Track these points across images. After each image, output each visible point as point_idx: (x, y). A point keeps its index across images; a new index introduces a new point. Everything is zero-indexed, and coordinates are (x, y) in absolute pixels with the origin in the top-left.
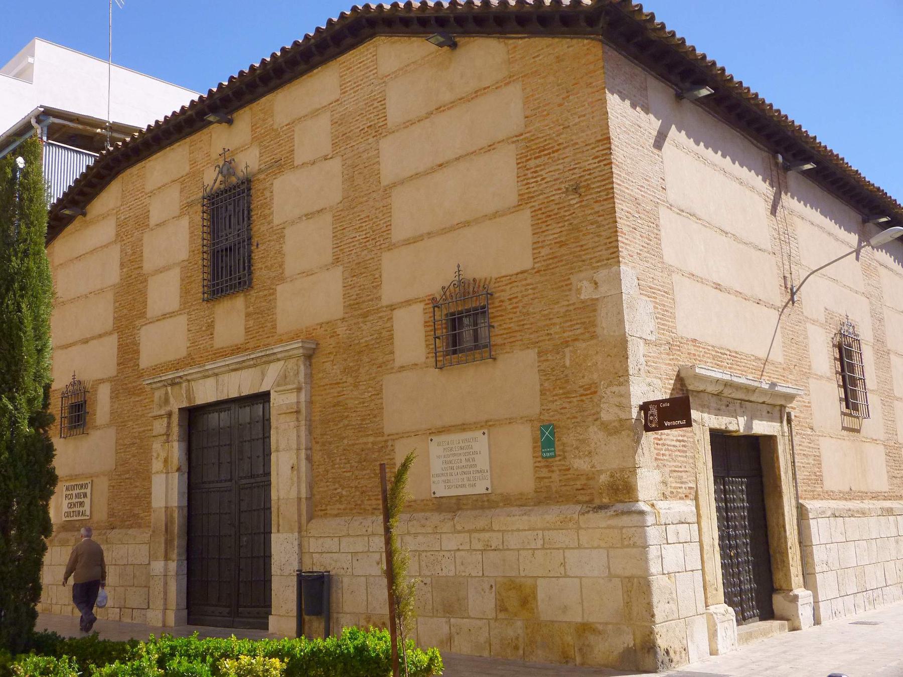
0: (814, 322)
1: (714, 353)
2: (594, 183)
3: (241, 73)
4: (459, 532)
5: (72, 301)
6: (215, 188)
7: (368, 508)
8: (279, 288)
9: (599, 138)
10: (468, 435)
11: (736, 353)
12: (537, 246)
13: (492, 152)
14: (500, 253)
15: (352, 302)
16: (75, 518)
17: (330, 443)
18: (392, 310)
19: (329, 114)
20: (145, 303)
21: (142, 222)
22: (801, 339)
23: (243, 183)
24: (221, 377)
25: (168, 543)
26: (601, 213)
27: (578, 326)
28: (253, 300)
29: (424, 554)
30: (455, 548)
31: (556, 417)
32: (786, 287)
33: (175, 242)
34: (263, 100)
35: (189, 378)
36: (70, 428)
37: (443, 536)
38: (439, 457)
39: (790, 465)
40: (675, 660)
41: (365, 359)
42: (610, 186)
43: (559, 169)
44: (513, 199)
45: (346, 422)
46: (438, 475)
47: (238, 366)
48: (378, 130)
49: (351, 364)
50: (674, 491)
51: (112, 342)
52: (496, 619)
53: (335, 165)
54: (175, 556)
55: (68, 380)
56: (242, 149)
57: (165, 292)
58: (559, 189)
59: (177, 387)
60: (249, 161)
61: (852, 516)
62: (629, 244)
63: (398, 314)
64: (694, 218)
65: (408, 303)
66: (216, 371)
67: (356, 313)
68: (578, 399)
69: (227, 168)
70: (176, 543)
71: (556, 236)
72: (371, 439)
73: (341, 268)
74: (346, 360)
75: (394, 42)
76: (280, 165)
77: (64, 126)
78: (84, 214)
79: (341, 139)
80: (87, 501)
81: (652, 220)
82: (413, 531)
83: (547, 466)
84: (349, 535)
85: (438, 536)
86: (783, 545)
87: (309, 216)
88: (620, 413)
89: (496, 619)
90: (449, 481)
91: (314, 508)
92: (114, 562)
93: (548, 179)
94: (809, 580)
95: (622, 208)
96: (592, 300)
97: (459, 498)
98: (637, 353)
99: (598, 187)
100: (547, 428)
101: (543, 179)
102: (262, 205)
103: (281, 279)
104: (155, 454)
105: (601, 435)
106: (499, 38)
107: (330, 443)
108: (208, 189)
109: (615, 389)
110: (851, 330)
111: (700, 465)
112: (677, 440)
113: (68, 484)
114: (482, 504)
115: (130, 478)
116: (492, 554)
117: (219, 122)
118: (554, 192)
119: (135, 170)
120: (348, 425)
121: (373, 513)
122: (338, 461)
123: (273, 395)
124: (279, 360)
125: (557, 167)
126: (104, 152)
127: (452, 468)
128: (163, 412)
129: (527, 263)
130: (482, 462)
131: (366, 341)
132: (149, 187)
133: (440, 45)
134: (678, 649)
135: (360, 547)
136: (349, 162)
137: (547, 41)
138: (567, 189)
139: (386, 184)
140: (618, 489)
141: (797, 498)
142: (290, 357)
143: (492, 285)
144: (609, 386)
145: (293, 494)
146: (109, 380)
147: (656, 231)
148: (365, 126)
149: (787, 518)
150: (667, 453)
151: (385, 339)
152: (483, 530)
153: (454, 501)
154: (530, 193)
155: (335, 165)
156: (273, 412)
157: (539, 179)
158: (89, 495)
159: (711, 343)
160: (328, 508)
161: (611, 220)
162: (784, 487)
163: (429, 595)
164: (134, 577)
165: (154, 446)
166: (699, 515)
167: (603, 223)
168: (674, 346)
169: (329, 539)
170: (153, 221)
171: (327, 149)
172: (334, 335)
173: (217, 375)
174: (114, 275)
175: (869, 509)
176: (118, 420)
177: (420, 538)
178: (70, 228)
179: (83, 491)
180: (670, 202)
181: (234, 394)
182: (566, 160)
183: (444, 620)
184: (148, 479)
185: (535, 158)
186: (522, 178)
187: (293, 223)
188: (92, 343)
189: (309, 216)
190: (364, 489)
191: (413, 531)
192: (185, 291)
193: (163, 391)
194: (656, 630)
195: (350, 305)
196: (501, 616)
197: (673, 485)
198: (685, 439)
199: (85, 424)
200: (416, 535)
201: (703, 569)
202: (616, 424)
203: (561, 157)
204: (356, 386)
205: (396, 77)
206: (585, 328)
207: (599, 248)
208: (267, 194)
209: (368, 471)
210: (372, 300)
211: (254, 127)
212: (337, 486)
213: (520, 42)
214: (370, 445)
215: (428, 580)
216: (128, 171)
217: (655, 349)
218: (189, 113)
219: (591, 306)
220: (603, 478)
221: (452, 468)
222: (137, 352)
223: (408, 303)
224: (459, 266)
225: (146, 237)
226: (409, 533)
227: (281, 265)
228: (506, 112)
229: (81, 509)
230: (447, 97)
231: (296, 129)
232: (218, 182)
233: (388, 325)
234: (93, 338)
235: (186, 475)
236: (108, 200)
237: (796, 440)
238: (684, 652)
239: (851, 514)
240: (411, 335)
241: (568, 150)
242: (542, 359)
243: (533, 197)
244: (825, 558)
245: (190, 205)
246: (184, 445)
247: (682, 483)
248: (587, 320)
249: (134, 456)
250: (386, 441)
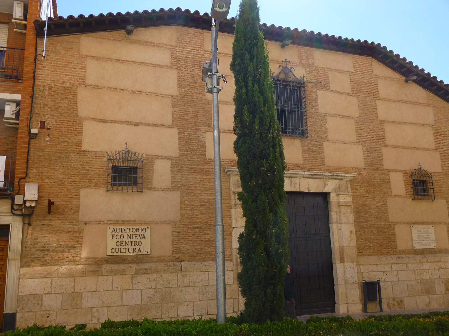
3: (366, 42)
4: (429, 262)
7: (384, 252)
17: (362, 222)
24: (293, 180)
28: (306, 144)
29: (416, 271)
30: (428, 268)
37: (424, 264)
41: (377, 189)
45: (370, 214)
47: (310, 176)
49: (371, 189)
52: (445, 294)
72: (383, 223)
82: (411, 262)
84: (381, 264)
85: (421, 264)
89: (445, 294)
90: (420, 243)
92: (191, 284)
97: (423, 250)
107: (362, 222)
114: (432, 252)
116: (442, 270)
122: (367, 230)
130: (432, 236)
131: (377, 181)
146: (169, 158)
151: (386, 183)
152: (438, 262)
153: (421, 250)
160: (364, 251)
163: (420, 287)
169: (371, 266)
173: (291, 177)
177: (414, 265)
183: (427, 296)
191: (411, 262)
200: (412, 263)
204: (374, 199)
209: (383, 237)
210: (379, 164)
212: (367, 242)
214: (383, 226)
215: (419, 281)
226: (409, 263)
240: (399, 185)
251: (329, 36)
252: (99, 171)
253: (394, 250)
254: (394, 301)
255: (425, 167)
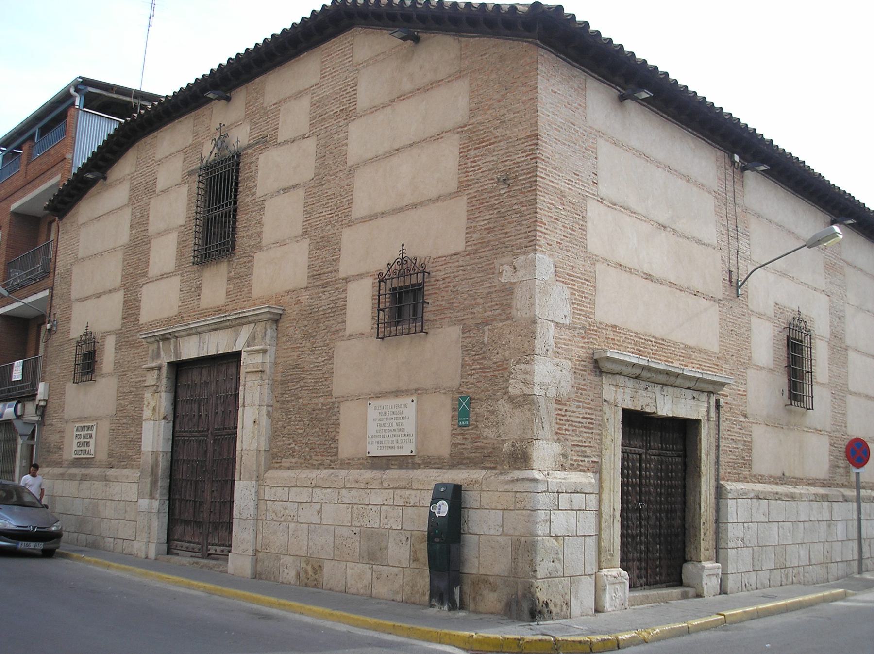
0: (760, 315)
1: (636, 339)
2: (521, 176)
5: (90, 257)
6: (210, 160)
8: (256, 256)
9: (529, 134)
10: (399, 401)
11: (663, 340)
12: (470, 230)
13: (440, 140)
14: (438, 236)
15: (315, 273)
16: (82, 456)
17: (288, 401)
18: (347, 282)
19: (309, 96)
20: (147, 262)
21: (150, 189)
22: (743, 330)
23: (233, 157)
25: (154, 483)
26: (525, 203)
27: (497, 307)
29: (356, 507)
31: (473, 390)
32: (730, 281)
33: (175, 208)
34: (257, 79)
35: (176, 334)
36: (83, 375)
38: (374, 420)
39: (714, 448)
40: (554, 613)
42: (534, 179)
43: (493, 161)
44: (453, 186)
45: (302, 383)
46: (373, 437)
48: (349, 114)
50: (576, 463)
51: (118, 298)
53: (311, 145)
54: (158, 496)
55: (82, 331)
56: (236, 125)
57: (165, 253)
58: (493, 179)
59: (167, 342)
60: (240, 137)
61: (780, 499)
62: (550, 233)
63: (352, 286)
64: (628, 212)
65: (361, 276)
66: (199, 330)
67: (317, 283)
68: (492, 374)
69: (221, 142)
70: (159, 484)
71: (486, 222)
72: (322, 400)
73: (308, 241)
74: (306, 326)
75: (369, 34)
76: (264, 142)
77: (100, 95)
78: (105, 178)
79: (317, 120)
80: (92, 441)
81: (579, 212)
83: (462, 434)
86: (697, 522)
87: (285, 190)
88: (524, 388)
90: (381, 442)
91: (274, 457)
93: (484, 169)
94: (718, 553)
95: (544, 200)
96: (511, 283)
98: (547, 335)
99: (524, 179)
100: (464, 398)
101: (480, 169)
102: (248, 178)
103: (259, 247)
104: (146, 403)
105: (508, 407)
106: (454, 35)
108: (205, 161)
109: (523, 366)
110: (803, 324)
111: (607, 441)
112: (583, 418)
113: (78, 425)
115: (127, 422)
116: (410, 510)
117: (219, 99)
118: (488, 182)
119: (148, 139)
120: (303, 387)
121: (318, 469)
123: (243, 354)
124: (250, 323)
125: (492, 158)
126: (128, 119)
127: (385, 431)
128: (154, 364)
129: (460, 246)
130: (410, 427)
132: (158, 157)
133: (404, 39)
134: (559, 603)
135: (304, 497)
136: (323, 142)
137: (493, 41)
138: (499, 179)
139: (352, 163)
140: (517, 458)
141: (717, 480)
142: (260, 321)
143: (430, 265)
144: (517, 363)
145: (254, 446)
147: (581, 223)
148: (338, 110)
149: (702, 497)
150: (570, 428)
151: (339, 309)
154: (468, 180)
155: (311, 145)
156: (243, 370)
157: (476, 168)
158: (94, 436)
159: (635, 330)
161: (532, 211)
162: (703, 468)
163: (358, 544)
164: (126, 511)
165: (146, 395)
166: (601, 487)
167: (526, 213)
168: (589, 330)
170: (160, 187)
171: (305, 129)
172: (298, 302)
173: (199, 333)
174: (124, 237)
175: (801, 494)
176: (121, 371)
177: (353, 492)
178: (94, 190)
179: (89, 432)
180: (602, 196)
181: (212, 352)
182: (500, 152)
184: (140, 425)
185: (475, 149)
186: (463, 169)
187: (272, 196)
188: (103, 298)
189: (285, 190)
190: (313, 445)
192: (180, 254)
193: (155, 345)
194: (536, 584)
195: (313, 276)
196: (413, 565)
197: (575, 458)
198: (593, 417)
199: (93, 371)
201: (599, 536)
202: (521, 399)
203: (497, 149)
205: (367, 66)
206: (502, 310)
207: (520, 236)
208: (253, 168)
211: (248, 104)
213: (471, 40)
214: (320, 406)
215: (357, 530)
216: (143, 140)
217: (567, 332)
218: (194, 89)
219: (508, 290)
220: (506, 447)
221: (385, 431)
222: (138, 308)
223: (361, 276)
224: (403, 245)
225: (153, 201)
227: (260, 234)
228: (452, 104)
229: (87, 449)
230: (407, 86)
231: (282, 109)
232: (213, 155)
233: (343, 296)
234: (104, 293)
235: (171, 424)
236: (126, 168)
237: (724, 426)
238: (565, 606)
239: (778, 497)
240: (360, 304)
241: (502, 143)
242: (465, 335)
243: (470, 185)
244: (742, 534)
245: (190, 174)
246: (170, 396)
247: (585, 457)
248: (505, 302)
249: (131, 404)
250: (333, 403)
251: (566, 11)
252: (672, 363)
253: (333, 458)
254: (307, 565)
255: (418, 251)
